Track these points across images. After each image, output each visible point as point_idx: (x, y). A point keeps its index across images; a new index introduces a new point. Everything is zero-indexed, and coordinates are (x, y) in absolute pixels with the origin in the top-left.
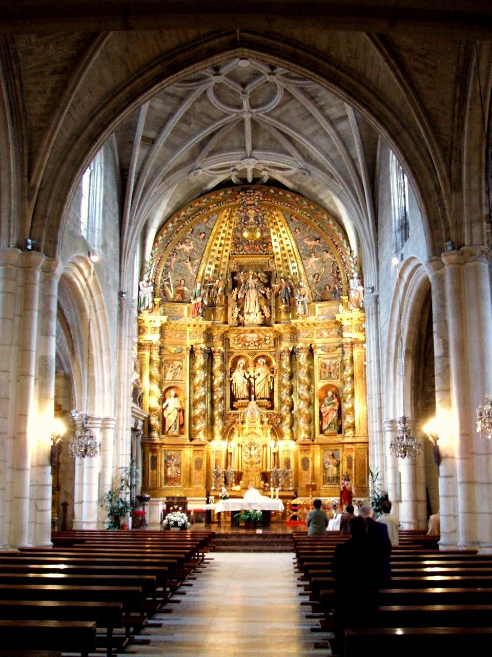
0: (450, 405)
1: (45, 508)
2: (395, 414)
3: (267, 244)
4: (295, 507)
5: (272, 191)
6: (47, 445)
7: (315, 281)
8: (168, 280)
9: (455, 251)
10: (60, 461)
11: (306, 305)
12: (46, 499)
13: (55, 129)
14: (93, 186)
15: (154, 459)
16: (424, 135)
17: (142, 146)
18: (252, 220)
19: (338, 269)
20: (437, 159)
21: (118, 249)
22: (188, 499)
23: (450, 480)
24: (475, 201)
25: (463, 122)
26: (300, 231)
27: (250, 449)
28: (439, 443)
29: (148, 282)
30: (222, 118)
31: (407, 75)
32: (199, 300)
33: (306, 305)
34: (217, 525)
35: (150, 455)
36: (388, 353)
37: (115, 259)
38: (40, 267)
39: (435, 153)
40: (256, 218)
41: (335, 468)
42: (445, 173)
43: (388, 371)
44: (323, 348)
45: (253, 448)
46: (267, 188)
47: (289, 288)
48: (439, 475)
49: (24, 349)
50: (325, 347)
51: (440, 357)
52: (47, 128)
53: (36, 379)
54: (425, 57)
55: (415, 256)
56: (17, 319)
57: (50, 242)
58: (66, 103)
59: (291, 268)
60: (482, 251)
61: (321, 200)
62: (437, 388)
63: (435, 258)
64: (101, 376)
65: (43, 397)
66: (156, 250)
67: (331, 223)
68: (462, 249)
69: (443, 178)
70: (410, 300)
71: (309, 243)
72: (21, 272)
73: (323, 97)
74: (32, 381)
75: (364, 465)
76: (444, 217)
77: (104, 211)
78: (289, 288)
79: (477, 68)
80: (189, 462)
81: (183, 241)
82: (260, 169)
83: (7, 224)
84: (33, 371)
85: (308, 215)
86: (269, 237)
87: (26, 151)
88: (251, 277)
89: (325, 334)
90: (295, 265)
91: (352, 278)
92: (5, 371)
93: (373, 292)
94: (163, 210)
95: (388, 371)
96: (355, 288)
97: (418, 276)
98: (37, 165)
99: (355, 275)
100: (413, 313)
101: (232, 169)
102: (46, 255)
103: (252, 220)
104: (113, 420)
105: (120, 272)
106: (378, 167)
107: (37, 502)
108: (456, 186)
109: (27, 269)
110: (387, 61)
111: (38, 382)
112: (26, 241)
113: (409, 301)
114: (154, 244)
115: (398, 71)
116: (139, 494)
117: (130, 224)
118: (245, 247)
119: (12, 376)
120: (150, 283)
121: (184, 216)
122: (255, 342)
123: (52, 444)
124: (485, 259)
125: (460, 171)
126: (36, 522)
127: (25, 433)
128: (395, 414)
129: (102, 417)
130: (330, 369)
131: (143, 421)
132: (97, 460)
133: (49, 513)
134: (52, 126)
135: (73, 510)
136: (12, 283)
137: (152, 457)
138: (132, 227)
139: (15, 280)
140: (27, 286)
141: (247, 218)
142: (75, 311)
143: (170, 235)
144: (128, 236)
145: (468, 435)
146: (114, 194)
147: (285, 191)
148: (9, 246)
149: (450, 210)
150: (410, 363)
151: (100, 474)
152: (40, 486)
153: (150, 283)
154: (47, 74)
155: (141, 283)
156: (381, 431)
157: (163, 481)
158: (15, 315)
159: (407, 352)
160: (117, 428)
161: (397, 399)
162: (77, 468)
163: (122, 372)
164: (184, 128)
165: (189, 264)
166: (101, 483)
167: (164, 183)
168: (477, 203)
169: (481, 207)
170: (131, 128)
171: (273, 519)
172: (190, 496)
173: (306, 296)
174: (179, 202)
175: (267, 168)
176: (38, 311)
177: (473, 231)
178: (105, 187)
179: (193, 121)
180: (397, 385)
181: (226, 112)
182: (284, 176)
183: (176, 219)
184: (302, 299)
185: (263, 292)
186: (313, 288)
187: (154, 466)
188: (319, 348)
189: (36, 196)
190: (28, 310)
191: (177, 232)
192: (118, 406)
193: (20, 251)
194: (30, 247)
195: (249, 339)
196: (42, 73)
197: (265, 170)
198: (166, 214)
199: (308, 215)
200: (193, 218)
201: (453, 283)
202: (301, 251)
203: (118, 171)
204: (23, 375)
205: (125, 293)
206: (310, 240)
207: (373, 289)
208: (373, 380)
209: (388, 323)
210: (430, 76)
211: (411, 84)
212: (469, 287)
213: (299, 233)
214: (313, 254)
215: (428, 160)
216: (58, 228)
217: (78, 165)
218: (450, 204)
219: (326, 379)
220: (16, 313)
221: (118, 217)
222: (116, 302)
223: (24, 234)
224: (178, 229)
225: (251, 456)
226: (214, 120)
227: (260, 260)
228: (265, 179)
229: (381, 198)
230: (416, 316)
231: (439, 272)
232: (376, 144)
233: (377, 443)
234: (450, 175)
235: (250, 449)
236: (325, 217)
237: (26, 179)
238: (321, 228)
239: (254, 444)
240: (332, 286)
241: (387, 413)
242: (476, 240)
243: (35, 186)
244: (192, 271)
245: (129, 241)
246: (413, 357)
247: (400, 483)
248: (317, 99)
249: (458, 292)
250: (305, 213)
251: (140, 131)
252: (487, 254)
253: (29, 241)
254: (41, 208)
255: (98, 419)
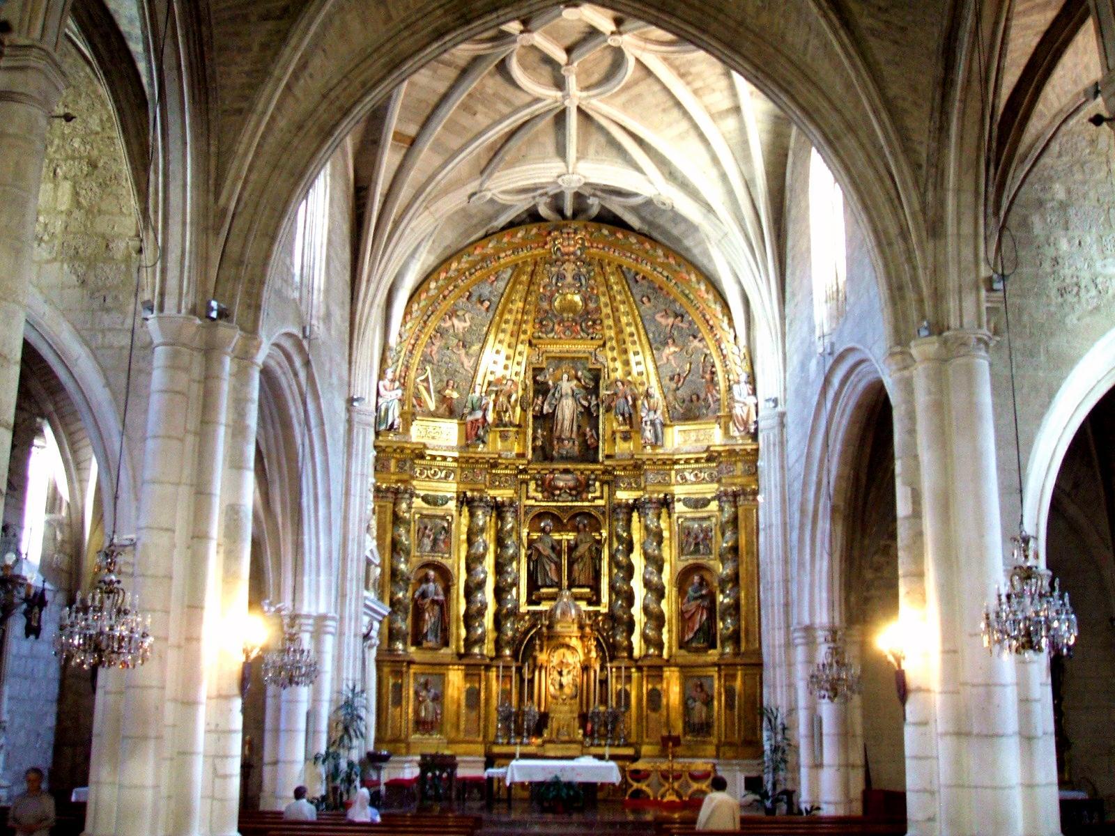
0: (924, 601)
1: (228, 772)
2: (812, 614)
3: (594, 322)
4: (638, 775)
5: (605, 232)
6: (235, 665)
7: (673, 385)
8: (427, 380)
9: (935, 338)
10: (258, 688)
11: (659, 427)
12: (232, 757)
13: (264, 113)
14: (317, 214)
15: (398, 689)
16: (882, 141)
17: (394, 147)
18: (569, 279)
19: (713, 366)
20: (904, 182)
21: (347, 324)
22: (458, 759)
23: (922, 729)
24: (967, 252)
25: (948, 121)
26: (649, 300)
27: (560, 673)
28: (904, 666)
29: (393, 381)
30: (529, 105)
31: (858, 42)
32: (479, 415)
33: (659, 427)
34: (505, 805)
35: (391, 681)
36: (803, 511)
37: (342, 341)
38: (230, 350)
39: (900, 172)
40: (577, 277)
41: (704, 709)
42: (917, 206)
43: (801, 540)
44: (686, 502)
45: (565, 672)
46: (595, 225)
47: (629, 398)
48: (904, 718)
49: (201, 492)
50: (690, 499)
51: (906, 518)
52: (251, 110)
53: (219, 545)
54: (886, 10)
55: (858, 346)
56: (190, 439)
57: (249, 306)
58: (285, 68)
59: (633, 363)
60: (979, 340)
61: (687, 249)
62: (901, 572)
63: (898, 349)
64: (314, 542)
65: (229, 574)
66: (408, 326)
67: (703, 287)
68: (946, 334)
69: (913, 214)
70: (842, 422)
71: (663, 321)
72: (198, 358)
73: (699, 75)
74: (213, 546)
75: (754, 703)
76: (915, 279)
77: (328, 257)
78: (629, 398)
79: (976, 33)
80: (456, 695)
81: (453, 314)
82: (586, 194)
83: (177, 273)
84: (216, 529)
85: (665, 273)
86: (598, 309)
87: (213, 149)
88: (565, 376)
89: (691, 477)
90: (640, 358)
91: (738, 382)
92: (167, 530)
93: (776, 406)
94: (422, 259)
95: (801, 540)
96: (741, 399)
97: (860, 381)
98: (231, 174)
99: (743, 377)
100: (846, 443)
101: (540, 192)
102: (242, 329)
103: (569, 279)
104: (333, 619)
105: (350, 363)
106: (788, 194)
107: (217, 761)
108: (935, 229)
109: (210, 351)
110: (825, 16)
111: (222, 550)
112: (209, 303)
113: (839, 423)
114: (405, 317)
115: (842, 33)
116: (371, 748)
117: (368, 281)
118: (556, 327)
119: (181, 534)
120: (397, 384)
121: (458, 270)
122: (571, 489)
123: (243, 659)
124: (983, 353)
125: (942, 203)
126: (213, 798)
127: (198, 639)
128: (812, 614)
129: (314, 614)
130: (697, 537)
131: (380, 622)
132: (304, 692)
133: (765, 738)
134: (260, 107)
135: (261, 776)
136: (183, 378)
137: (395, 685)
138: (373, 287)
139: (187, 370)
140: (208, 380)
141: (561, 277)
142: (274, 428)
143: (433, 302)
144: (364, 302)
145: (955, 652)
146: (345, 228)
147: (626, 232)
148: (179, 311)
149: (925, 268)
150: (839, 529)
151: (308, 714)
152: (220, 732)
153: (397, 384)
154: (253, 19)
155: (381, 383)
156: (789, 645)
157: (411, 725)
158: (186, 431)
159: (834, 509)
160: (340, 634)
161: (816, 590)
162: (270, 702)
163: (351, 537)
164: (465, 120)
165: (463, 352)
166: (311, 729)
167: (426, 213)
168: (971, 257)
169: (977, 264)
170: (377, 118)
171: (600, 795)
172: (461, 755)
173: (659, 412)
174: (449, 246)
175: (599, 193)
176: (227, 426)
177: (964, 304)
178: (331, 216)
179: (480, 108)
180: (817, 567)
181: (537, 95)
182: (625, 207)
183: (443, 275)
184: (652, 416)
185: (585, 403)
186: (671, 398)
187: (398, 701)
188: (679, 500)
189: (227, 226)
190: (207, 423)
191: (445, 297)
192: (342, 595)
193: (198, 321)
194: (214, 314)
195: (561, 484)
196: (245, 18)
197: (594, 195)
198: (426, 266)
199: (665, 273)
200: (471, 274)
201: (929, 393)
202: (651, 336)
203: (352, 189)
204: (199, 536)
205: (357, 400)
206: (667, 315)
207: (776, 401)
208: (774, 556)
209: (804, 459)
210: (896, 42)
211: (863, 55)
212: (957, 400)
213: (648, 305)
214: (670, 341)
215: (888, 183)
216: (262, 283)
217: (297, 180)
218: (924, 258)
219: (691, 554)
220: (188, 427)
221: (349, 268)
222: (343, 415)
223: (205, 293)
224: (446, 292)
225: (561, 686)
226: (516, 110)
227: (582, 347)
228: (594, 211)
229: (794, 247)
230: (851, 449)
231: (906, 373)
232: (786, 155)
233: (780, 666)
234: (924, 210)
235: (560, 673)
236: (693, 278)
237: (211, 197)
238: (687, 296)
239: (568, 665)
240: (702, 396)
241: (800, 613)
242: (968, 319)
243: (224, 211)
244: (468, 364)
245: (366, 310)
246: (846, 518)
247: (821, 734)
248: (690, 78)
249: (939, 407)
250: (659, 269)
251: (394, 122)
252: (986, 344)
253: (214, 304)
254: (234, 249)
255: (308, 616)
